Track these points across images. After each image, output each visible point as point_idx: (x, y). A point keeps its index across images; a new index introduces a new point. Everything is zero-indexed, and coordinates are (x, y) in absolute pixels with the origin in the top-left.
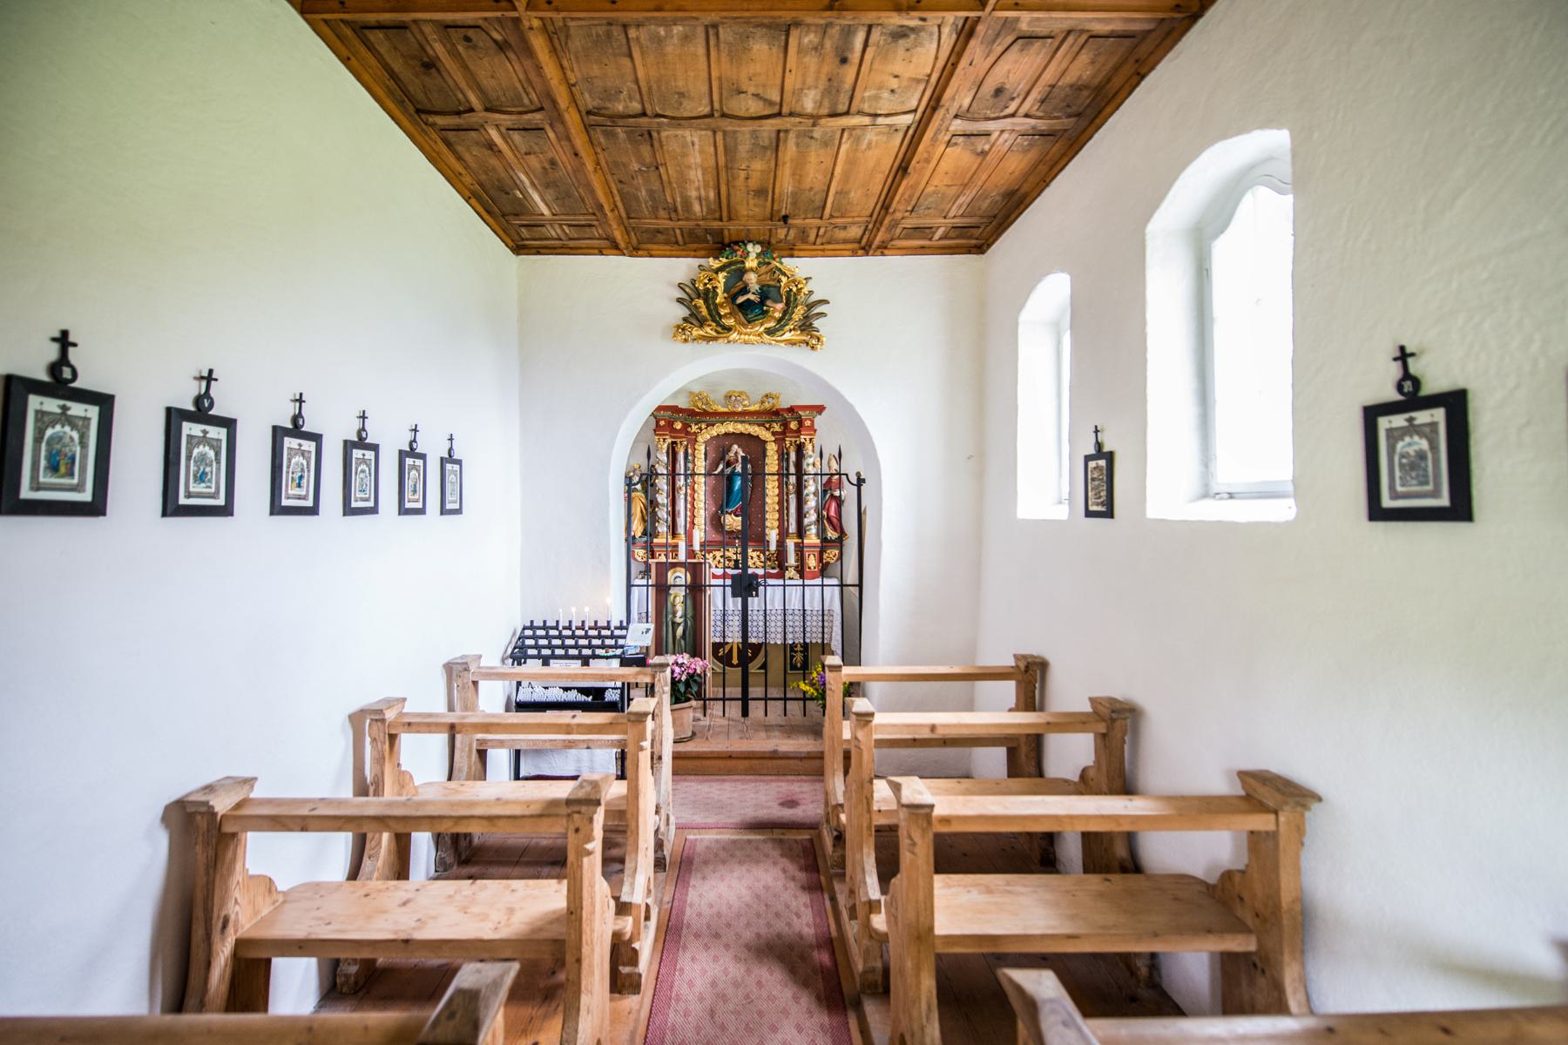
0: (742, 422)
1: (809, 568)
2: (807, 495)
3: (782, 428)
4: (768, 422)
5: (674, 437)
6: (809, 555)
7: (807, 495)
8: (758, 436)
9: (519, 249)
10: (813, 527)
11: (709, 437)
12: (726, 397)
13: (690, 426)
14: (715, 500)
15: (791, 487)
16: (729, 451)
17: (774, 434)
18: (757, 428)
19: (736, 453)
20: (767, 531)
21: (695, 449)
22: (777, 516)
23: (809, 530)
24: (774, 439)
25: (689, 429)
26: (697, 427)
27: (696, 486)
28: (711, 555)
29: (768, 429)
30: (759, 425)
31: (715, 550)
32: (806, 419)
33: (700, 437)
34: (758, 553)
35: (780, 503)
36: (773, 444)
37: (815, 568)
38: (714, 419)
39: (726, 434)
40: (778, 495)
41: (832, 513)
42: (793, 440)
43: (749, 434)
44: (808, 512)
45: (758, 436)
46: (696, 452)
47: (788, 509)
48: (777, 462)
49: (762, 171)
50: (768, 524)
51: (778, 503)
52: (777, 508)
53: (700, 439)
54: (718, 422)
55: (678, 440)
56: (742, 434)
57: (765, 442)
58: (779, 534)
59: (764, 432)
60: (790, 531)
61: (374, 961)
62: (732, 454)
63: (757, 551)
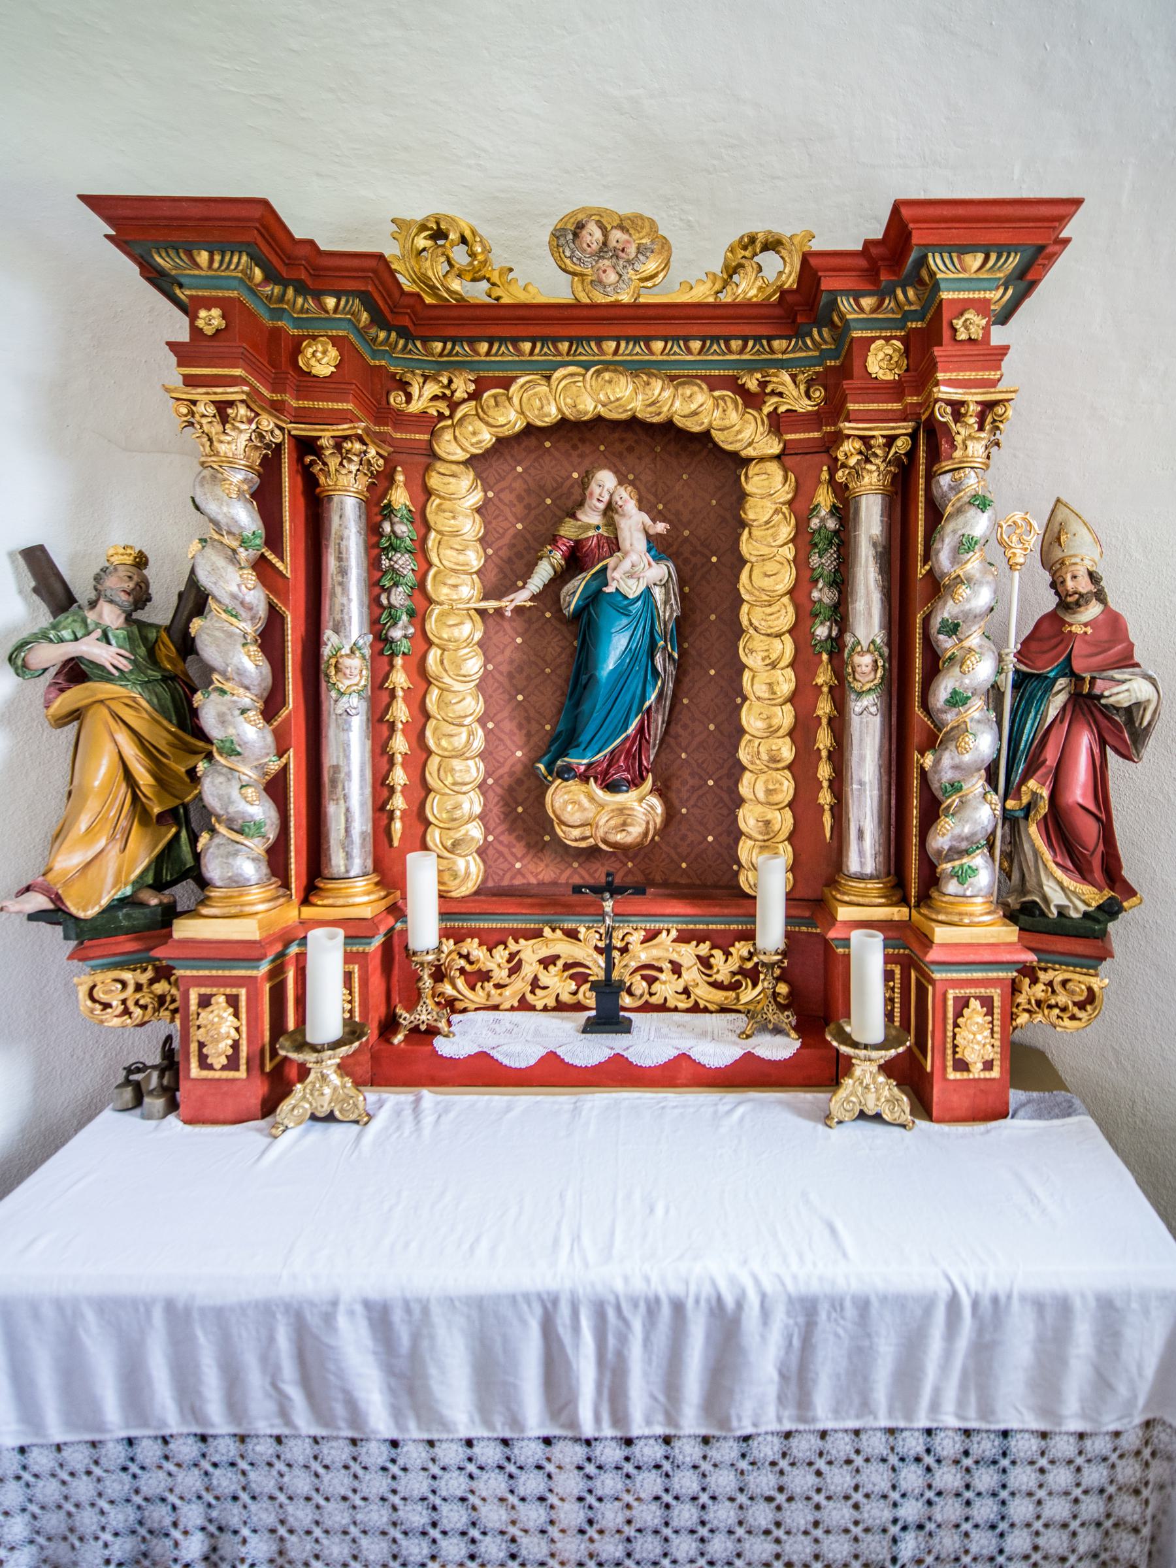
0: (635, 369)
1: (962, 1065)
2: (957, 700)
3: (818, 393)
4: (751, 367)
5: (300, 416)
6: (963, 1004)
7: (957, 700)
8: (706, 436)
9: (265, 203)
10: (979, 860)
11: (487, 438)
12: (557, 235)
13: (404, 386)
14: (526, 717)
15: (864, 662)
16: (581, 504)
17: (777, 423)
18: (700, 398)
19: (610, 510)
20: (745, 851)
21: (428, 493)
22: (786, 787)
23: (962, 876)
24: (776, 449)
25: (396, 399)
26: (432, 389)
27: (433, 656)
28: (501, 954)
29: (752, 400)
30: (713, 384)
31: (517, 935)
32: (963, 307)
33: (448, 436)
34: (704, 949)
35: (801, 733)
36: (774, 468)
37: (988, 1065)
38: (506, 353)
39: (563, 424)
40: (792, 699)
41: (1079, 790)
42: (878, 432)
43: (669, 426)
44: (956, 787)
45: (706, 436)
46: (435, 502)
47: (839, 757)
48: (789, 552)
49: (937, 384)
50: (748, 819)
51: (791, 734)
52: (787, 752)
53: (450, 447)
54: (529, 366)
55: (326, 437)
56: (633, 424)
57: (740, 461)
58: (792, 869)
59: (733, 416)
60: (853, 864)
61: (851, 1077)
62: (591, 517)
63: (700, 938)
